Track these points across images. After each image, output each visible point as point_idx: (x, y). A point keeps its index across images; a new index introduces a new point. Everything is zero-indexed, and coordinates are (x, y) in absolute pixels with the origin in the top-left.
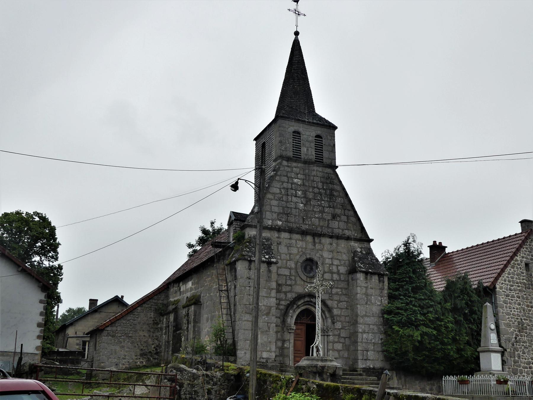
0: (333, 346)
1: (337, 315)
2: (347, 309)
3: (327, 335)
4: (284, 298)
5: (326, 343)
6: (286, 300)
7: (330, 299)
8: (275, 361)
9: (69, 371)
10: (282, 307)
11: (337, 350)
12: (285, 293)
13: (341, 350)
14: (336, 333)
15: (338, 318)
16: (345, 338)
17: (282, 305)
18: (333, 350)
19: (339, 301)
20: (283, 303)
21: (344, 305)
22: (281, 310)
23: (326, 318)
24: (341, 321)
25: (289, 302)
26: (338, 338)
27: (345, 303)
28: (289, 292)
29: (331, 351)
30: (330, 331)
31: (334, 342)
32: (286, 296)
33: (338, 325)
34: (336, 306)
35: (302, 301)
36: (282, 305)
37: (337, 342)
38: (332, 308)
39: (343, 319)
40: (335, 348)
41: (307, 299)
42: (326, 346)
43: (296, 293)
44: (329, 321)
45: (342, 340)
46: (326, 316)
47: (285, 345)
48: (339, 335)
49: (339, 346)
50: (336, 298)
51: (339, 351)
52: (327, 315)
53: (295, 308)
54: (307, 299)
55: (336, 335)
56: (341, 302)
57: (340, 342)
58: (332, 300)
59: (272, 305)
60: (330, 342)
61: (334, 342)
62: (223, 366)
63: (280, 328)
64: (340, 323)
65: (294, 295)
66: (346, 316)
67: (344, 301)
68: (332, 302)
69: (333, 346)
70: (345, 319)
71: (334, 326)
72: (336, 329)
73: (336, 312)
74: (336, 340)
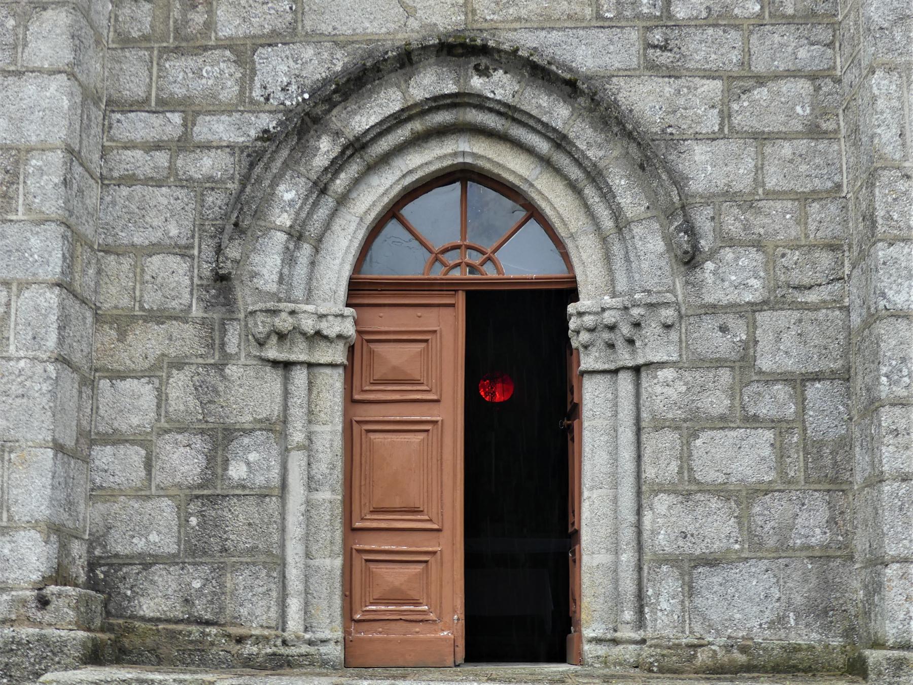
0: (685, 458)
1: (729, 196)
2: (814, 132)
3: (637, 370)
4: (229, 92)
5: (627, 435)
6: (245, 104)
7: (653, 68)
8: (43, 602)
9: (172, 636)
10: (208, 164)
11: (722, 492)
12: (243, 52)
13: (758, 491)
14: (713, 341)
15: (732, 223)
16: (799, 382)
17: (207, 147)
18: (688, 488)
19: (741, 80)
20: (219, 128)
21: (783, 104)
22: (201, 187)
23: (622, 224)
24: (758, 245)
25: (267, 122)
26: (733, 392)
27: (803, 87)
28: (272, 40)
29: (662, 503)
30: (652, 329)
31: (692, 425)
32: (249, 73)
33: (735, 277)
34: (712, 122)
35: (387, 101)
36: (207, 147)
37: (723, 422)
38: (673, 141)
39: (777, 220)
40: (708, 475)
41: (430, 82)
42: (627, 455)
43: (338, 43)
44: (651, 244)
45: (775, 401)
46: (617, 214)
47: (237, 471)
48: (743, 362)
49: (743, 456)
50: (700, 49)
51: (742, 497)
52: (631, 200)
53: (320, 161)
54: (430, 82)
55: (719, 363)
56: (760, 80)
57: (752, 421)
58: (672, 73)
59: (33, 134)
60: (660, 425)
61: (692, 425)
62: (157, 630)
63: (188, 331)
64: (751, 259)
65: (320, 64)
66: (805, 199)
67: (793, 74)
68: (668, 88)
69: (685, 458)
70: (802, 220)
71: (697, 286)
72: (713, 309)
73: (705, 167)
74: (716, 402)
